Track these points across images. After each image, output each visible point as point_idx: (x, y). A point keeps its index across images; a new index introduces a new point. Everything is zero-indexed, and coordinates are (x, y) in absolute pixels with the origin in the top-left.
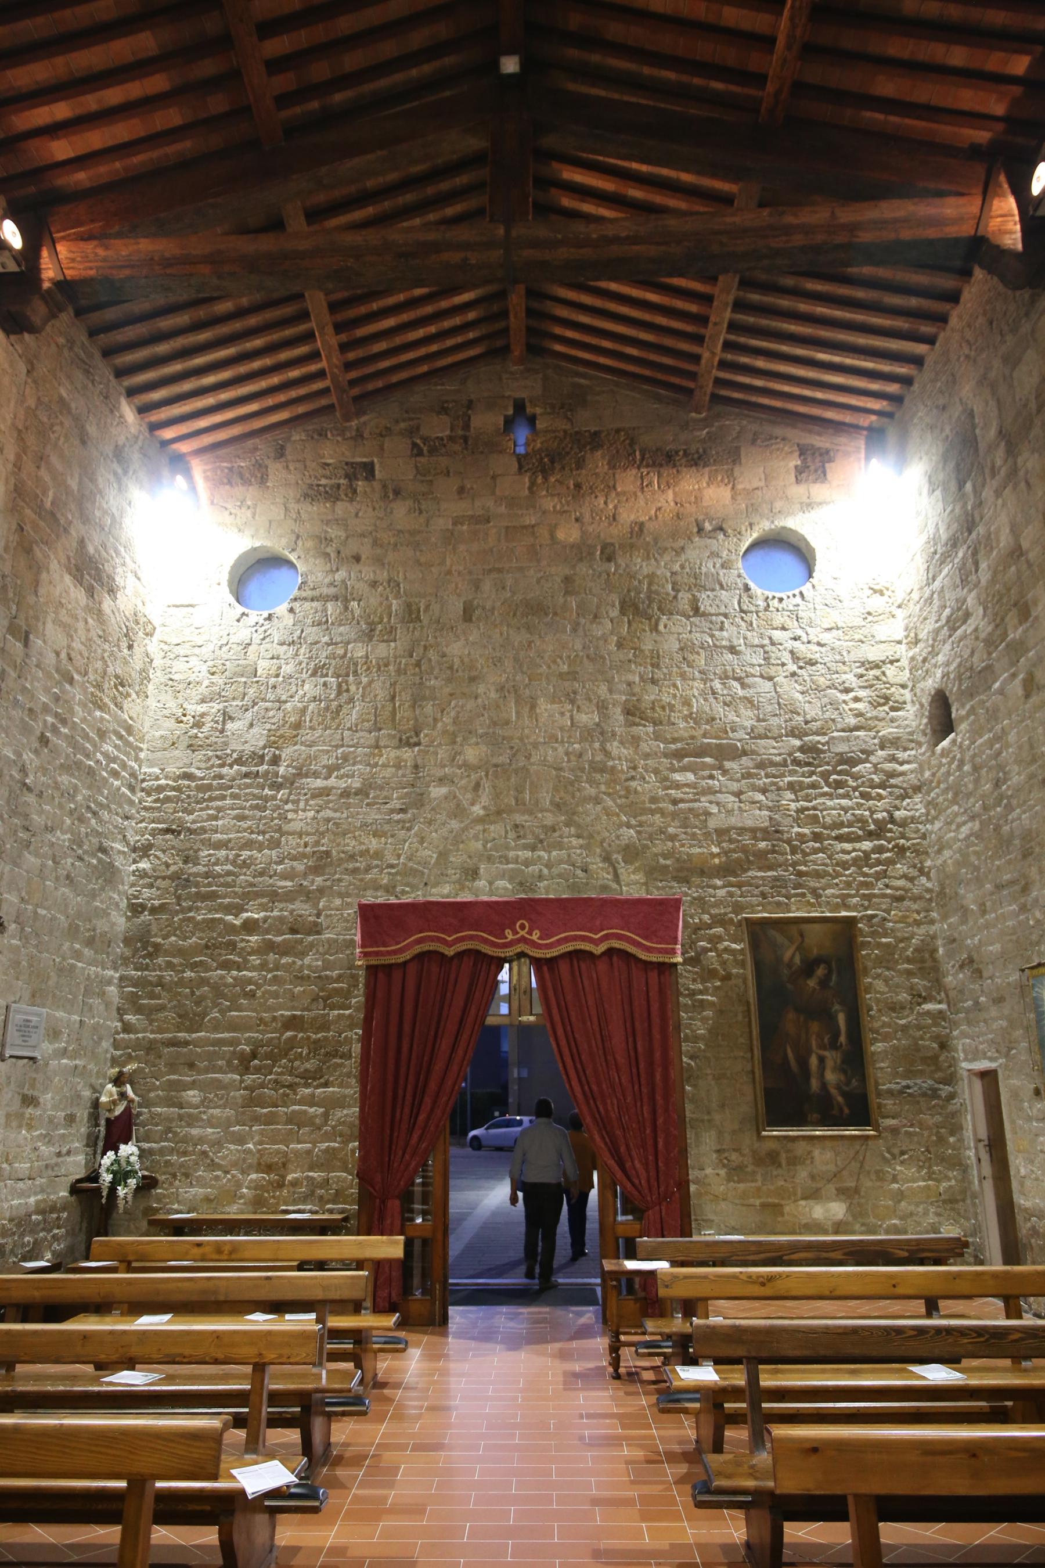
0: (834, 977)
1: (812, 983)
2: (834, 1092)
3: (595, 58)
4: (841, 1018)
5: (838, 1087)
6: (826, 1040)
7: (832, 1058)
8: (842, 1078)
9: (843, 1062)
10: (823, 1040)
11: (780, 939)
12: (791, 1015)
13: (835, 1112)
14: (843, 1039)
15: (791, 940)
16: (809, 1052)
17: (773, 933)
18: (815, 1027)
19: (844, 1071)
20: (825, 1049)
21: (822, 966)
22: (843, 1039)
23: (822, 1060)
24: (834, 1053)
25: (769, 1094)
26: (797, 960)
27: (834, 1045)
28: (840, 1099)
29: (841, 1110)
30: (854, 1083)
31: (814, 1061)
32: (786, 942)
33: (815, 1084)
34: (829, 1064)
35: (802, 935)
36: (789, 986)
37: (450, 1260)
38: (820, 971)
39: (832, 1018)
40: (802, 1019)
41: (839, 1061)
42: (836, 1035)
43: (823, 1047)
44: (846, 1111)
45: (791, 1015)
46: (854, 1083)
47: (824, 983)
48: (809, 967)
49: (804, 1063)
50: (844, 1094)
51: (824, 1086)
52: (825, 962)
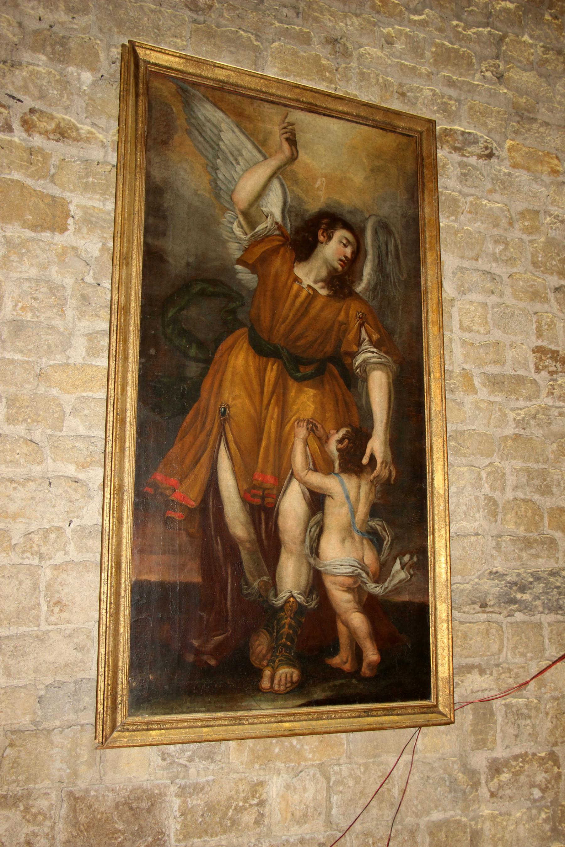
0: (368, 270)
1: (309, 275)
2: (342, 599)
3: (263, 523)
4: (378, 389)
5: (355, 588)
6: (333, 447)
7: (348, 496)
8: (369, 557)
9: (374, 511)
10: (323, 441)
11: (230, 136)
12: (239, 360)
13: (341, 660)
14: (377, 445)
15: (261, 145)
16: (283, 475)
17: (208, 112)
18: (306, 401)
19: (375, 539)
20: (329, 471)
21: (340, 234)
22: (377, 445)
23: (317, 501)
24: (351, 482)
25: (152, 606)
26: (273, 205)
27: (353, 461)
28: (358, 620)
29: (358, 653)
30: (399, 573)
31: (292, 506)
32: (249, 150)
33: (291, 576)
34: (336, 515)
35: (292, 141)
36: (245, 275)
37: (289, 377)
38: (333, 249)
39: (353, 382)
40: (271, 374)
41: (362, 510)
42: (359, 436)
43: (321, 464)
44: (371, 655)
45: (239, 360)
46: (399, 573)
47: (340, 281)
48: (303, 237)
49: (263, 512)
50: (370, 606)
51: (316, 582)
52: (347, 226)
